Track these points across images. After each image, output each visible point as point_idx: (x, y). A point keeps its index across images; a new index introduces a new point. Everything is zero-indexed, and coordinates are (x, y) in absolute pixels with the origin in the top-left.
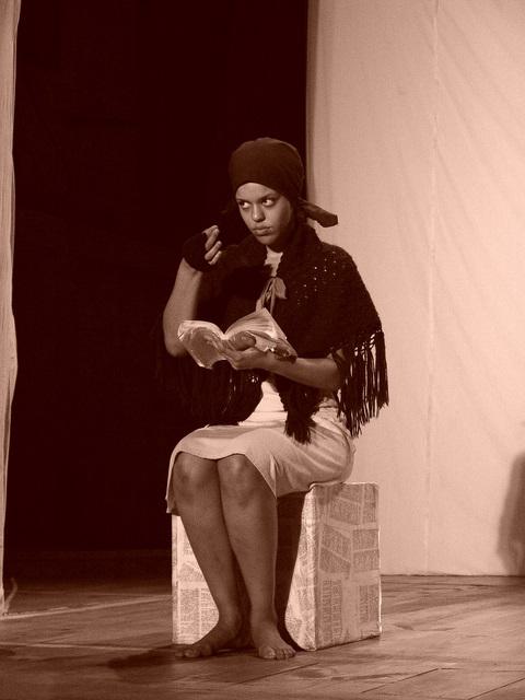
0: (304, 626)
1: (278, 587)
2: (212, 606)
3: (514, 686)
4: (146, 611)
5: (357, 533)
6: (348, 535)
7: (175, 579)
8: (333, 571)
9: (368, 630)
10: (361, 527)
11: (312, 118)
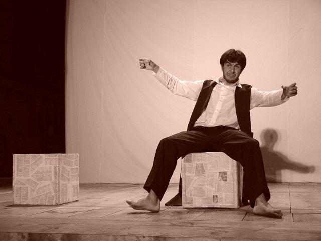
0: (55, 197)
1: (126, 187)
2: (137, 202)
3: (116, 214)
4: (295, 227)
5: (72, 169)
6: (69, 170)
7: (13, 185)
8: (65, 181)
9: (76, 198)
10: (73, 167)
11: (70, 15)
